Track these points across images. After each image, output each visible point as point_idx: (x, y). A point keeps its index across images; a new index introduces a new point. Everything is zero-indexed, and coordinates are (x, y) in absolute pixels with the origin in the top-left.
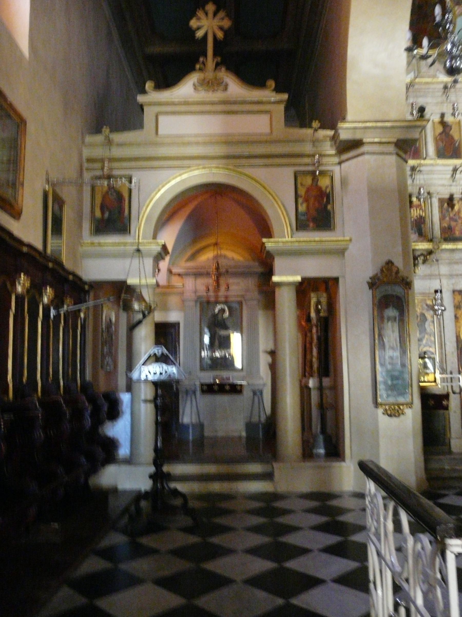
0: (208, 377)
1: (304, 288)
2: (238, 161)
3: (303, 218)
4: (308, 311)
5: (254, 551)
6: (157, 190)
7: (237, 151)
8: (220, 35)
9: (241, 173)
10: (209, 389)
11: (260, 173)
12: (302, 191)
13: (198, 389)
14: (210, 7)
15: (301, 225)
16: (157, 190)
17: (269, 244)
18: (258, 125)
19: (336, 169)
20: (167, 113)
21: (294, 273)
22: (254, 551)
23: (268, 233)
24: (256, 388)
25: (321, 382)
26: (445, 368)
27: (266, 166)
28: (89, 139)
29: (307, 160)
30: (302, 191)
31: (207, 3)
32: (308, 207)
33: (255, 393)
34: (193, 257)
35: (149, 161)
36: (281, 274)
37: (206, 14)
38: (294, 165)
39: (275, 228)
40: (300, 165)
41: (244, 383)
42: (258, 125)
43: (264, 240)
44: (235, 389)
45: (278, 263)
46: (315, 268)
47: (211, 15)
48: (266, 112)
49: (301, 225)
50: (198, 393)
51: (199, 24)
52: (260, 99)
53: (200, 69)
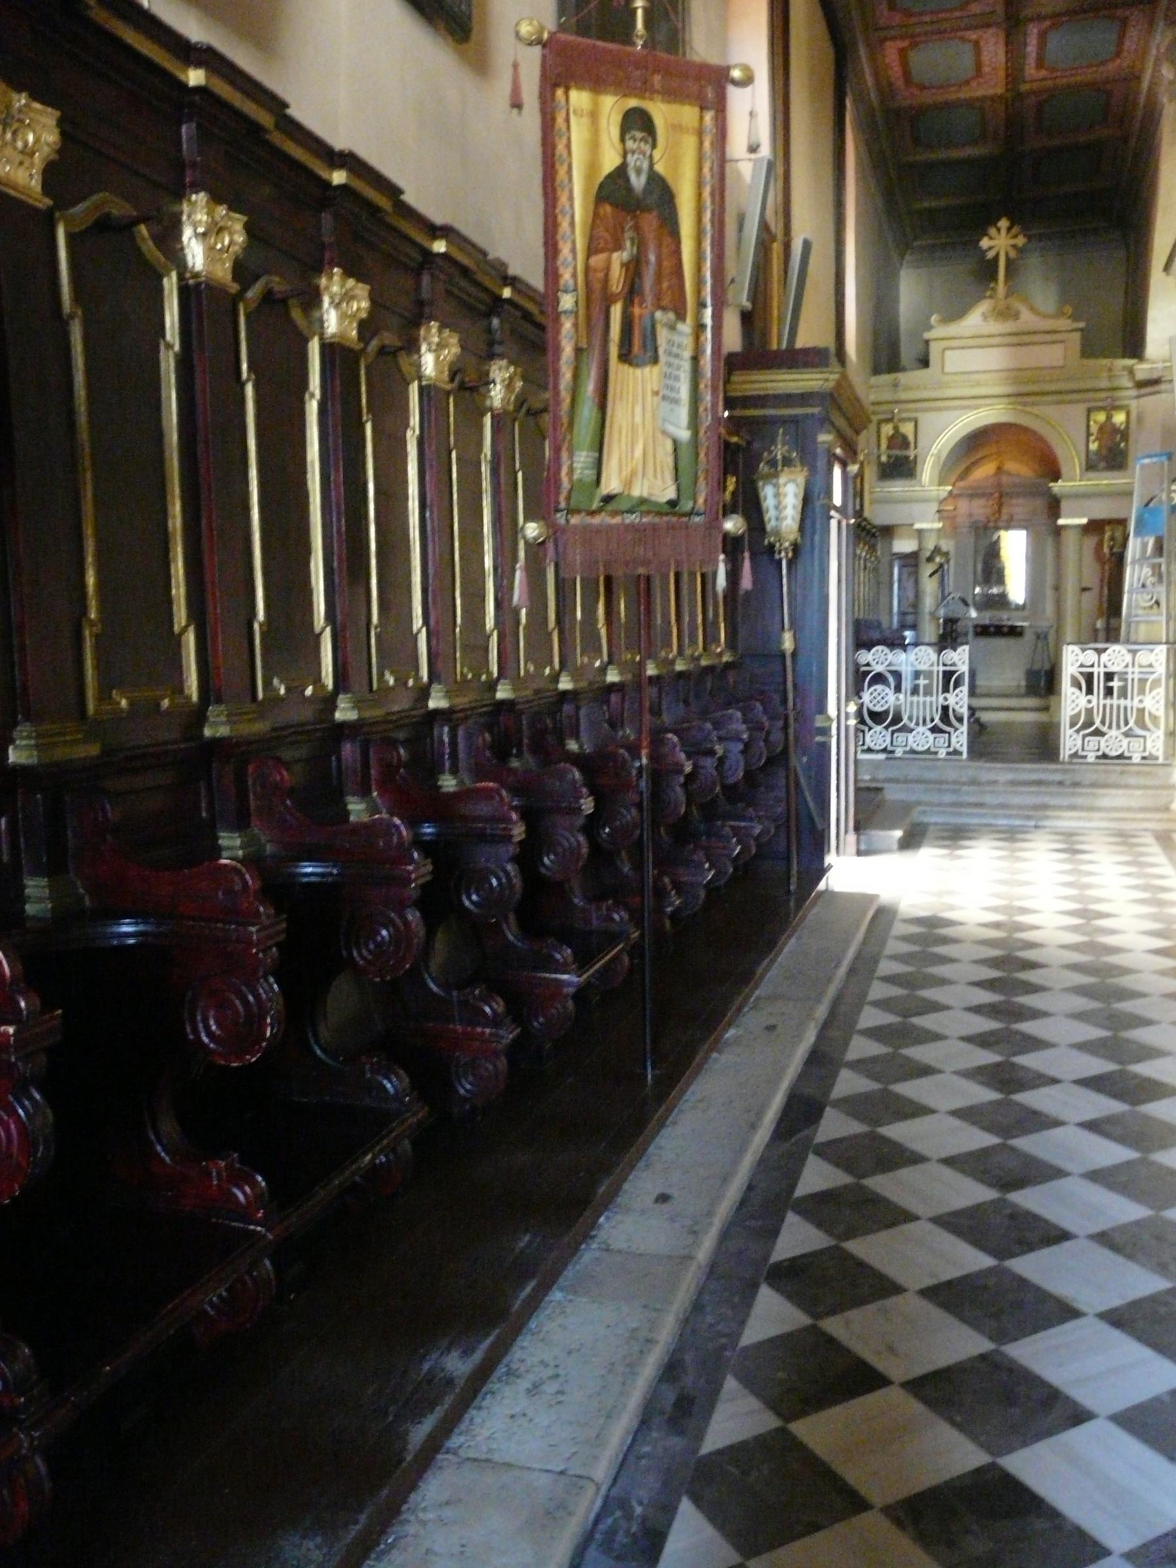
0: (987, 618)
1: (1094, 527)
2: (1027, 399)
3: (1094, 457)
4: (786, 1146)
5: (967, 1114)
6: (941, 435)
7: (1027, 388)
8: (1013, 254)
9: (1030, 413)
10: (983, 631)
11: (1050, 411)
12: (1094, 428)
13: (971, 630)
14: (1004, 223)
15: (1090, 466)
16: (941, 435)
17: (1057, 487)
18: (1051, 355)
19: (1133, 404)
20: (952, 348)
21: (1083, 516)
22: (967, 1114)
23: (1056, 476)
24: (1039, 631)
25: (1108, 623)
26: (489, 709)
27: (1058, 403)
28: (874, 380)
29: (1102, 395)
30: (1094, 428)
31: (998, 219)
32: (1100, 446)
33: (1038, 637)
34: (963, 476)
35: (936, 403)
36: (1068, 517)
37: (999, 230)
38: (1089, 401)
39: (1064, 470)
40: (1094, 400)
41: (1025, 624)
42: (1051, 355)
43: (1051, 484)
44: (1014, 632)
45: (1064, 505)
46: (1102, 510)
47: (1003, 232)
48: (1062, 342)
49: (1090, 466)
50: (970, 636)
51: (992, 243)
52: (1054, 328)
53: (991, 297)
